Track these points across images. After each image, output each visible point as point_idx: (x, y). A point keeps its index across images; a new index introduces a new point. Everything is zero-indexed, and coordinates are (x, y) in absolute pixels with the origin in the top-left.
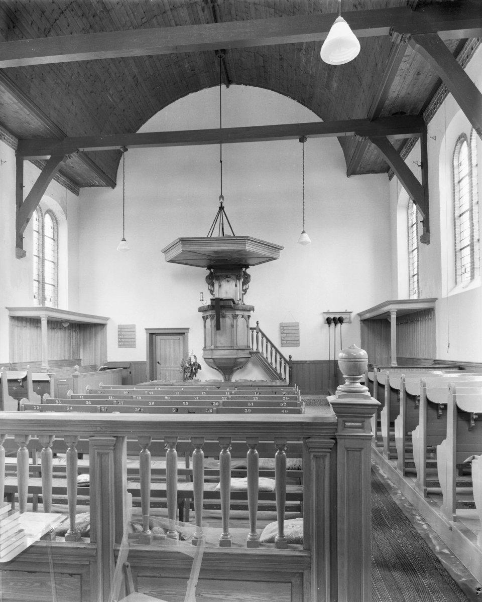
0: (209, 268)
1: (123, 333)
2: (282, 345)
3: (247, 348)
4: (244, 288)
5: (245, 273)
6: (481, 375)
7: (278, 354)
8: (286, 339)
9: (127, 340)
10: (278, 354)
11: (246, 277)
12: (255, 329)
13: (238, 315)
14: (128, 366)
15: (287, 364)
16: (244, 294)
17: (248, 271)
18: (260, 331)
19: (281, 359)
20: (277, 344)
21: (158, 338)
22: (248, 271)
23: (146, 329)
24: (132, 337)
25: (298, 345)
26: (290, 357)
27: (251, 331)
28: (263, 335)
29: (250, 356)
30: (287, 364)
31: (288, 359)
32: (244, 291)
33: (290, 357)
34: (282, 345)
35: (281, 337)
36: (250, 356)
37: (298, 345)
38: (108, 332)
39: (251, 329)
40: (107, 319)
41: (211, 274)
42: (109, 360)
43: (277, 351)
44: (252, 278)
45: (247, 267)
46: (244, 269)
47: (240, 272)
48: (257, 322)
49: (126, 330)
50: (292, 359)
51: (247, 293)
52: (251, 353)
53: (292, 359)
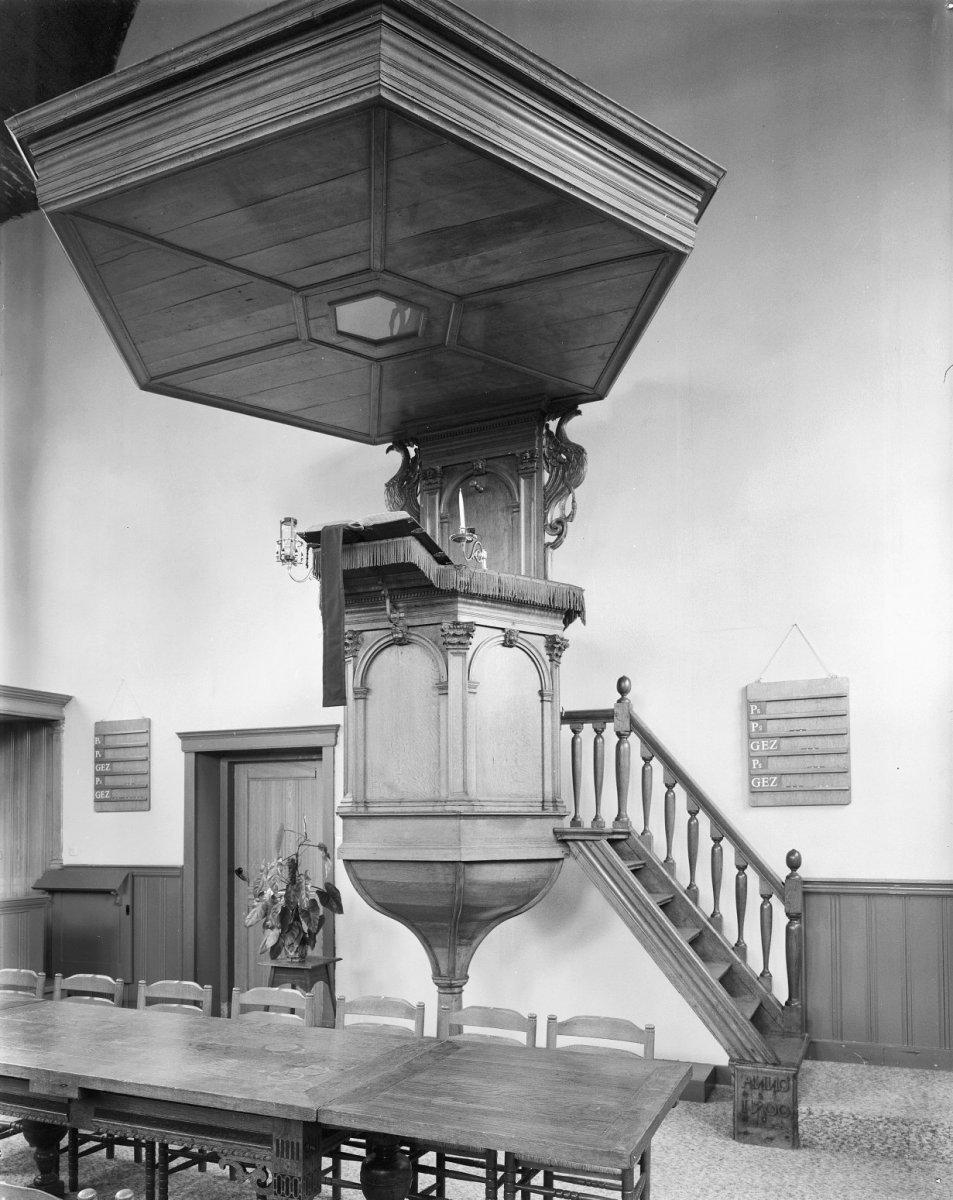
0: (400, 445)
1: (109, 754)
2: (757, 796)
3: (538, 810)
4: (555, 514)
5: (559, 440)
6: (2, 712)
7: (725, 843)
8: (776, 765)
9: (120, 781)
10: (725, 843)
11: (561, 462)
12: (599, 718)
13: (469, 630)
14: (114, 884)
15: (775, 900)
16: (554, 546)
17: (575, 429)
18: (635, 726)
19: (741, 869)
20: (724, 786)
21: (243, 771)
22: (575, 429)
23: (184, 736)
24: (139, 767)
25: (839, 796)
26: (793, 862)
27: (567, 728)
28: (653, 748)
29: (557, 852)
30: (775, 900)
31: (782, 872)
32: (553, 528)
33: (793, 862)
34: (757, 796)
35: (751, 757)
36: (557, 852)
37: (839, 796)
38: (65, 752)
39: (574, 719)
40: (63, 701)
41: (408, 465)
42: (68, 859)
43: (722, 829)
44: (592, 468)
45: (568, 408)
46: (553, 425)
47: (532, 437)
48: (621, 680)
49: (120, 741)
50: (803, 872)
51: (567, 541)
52: (562, 839)
53: (803, 872)
